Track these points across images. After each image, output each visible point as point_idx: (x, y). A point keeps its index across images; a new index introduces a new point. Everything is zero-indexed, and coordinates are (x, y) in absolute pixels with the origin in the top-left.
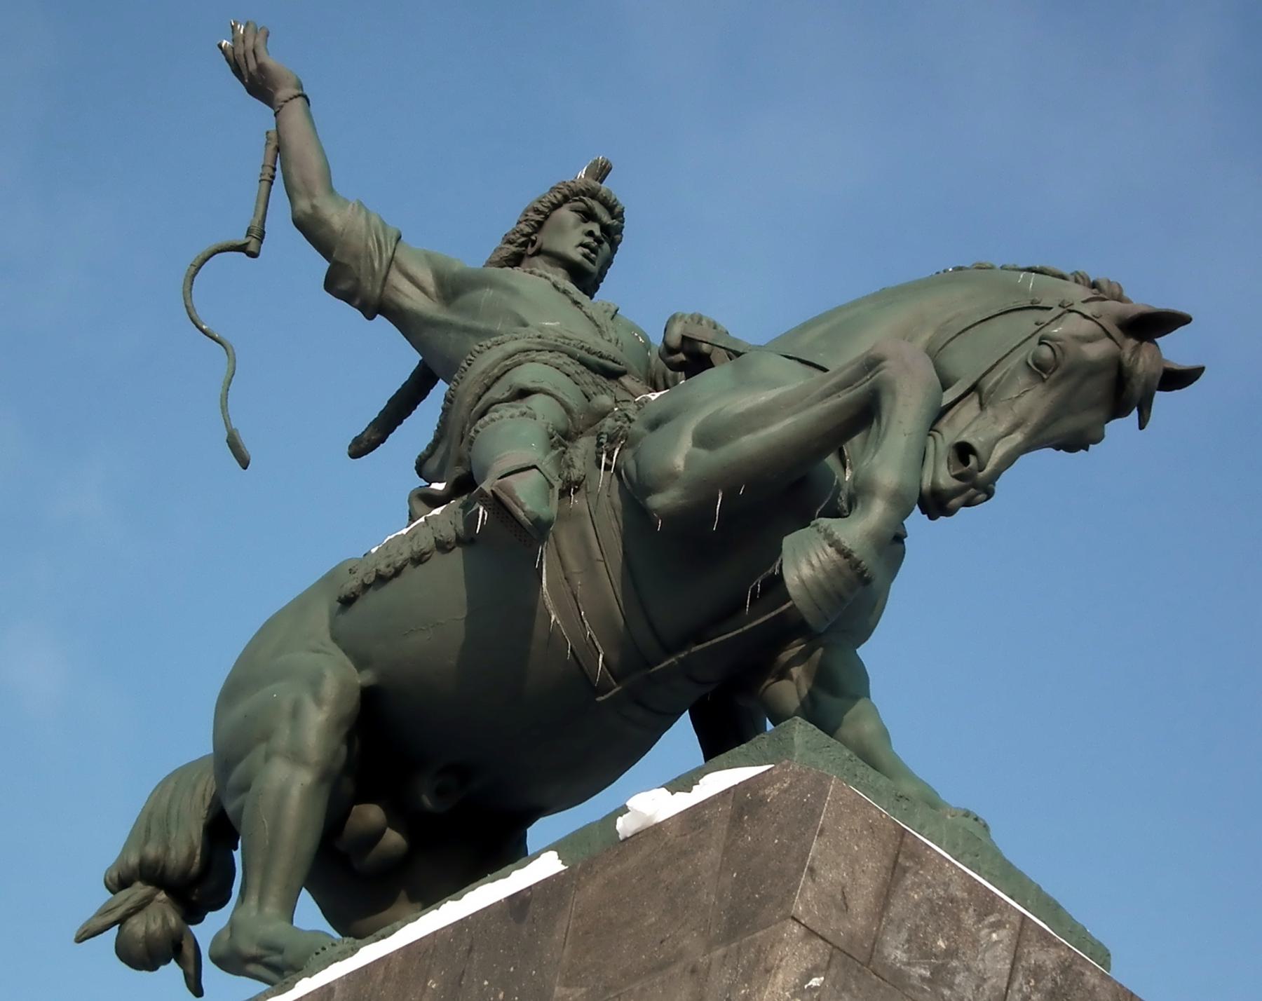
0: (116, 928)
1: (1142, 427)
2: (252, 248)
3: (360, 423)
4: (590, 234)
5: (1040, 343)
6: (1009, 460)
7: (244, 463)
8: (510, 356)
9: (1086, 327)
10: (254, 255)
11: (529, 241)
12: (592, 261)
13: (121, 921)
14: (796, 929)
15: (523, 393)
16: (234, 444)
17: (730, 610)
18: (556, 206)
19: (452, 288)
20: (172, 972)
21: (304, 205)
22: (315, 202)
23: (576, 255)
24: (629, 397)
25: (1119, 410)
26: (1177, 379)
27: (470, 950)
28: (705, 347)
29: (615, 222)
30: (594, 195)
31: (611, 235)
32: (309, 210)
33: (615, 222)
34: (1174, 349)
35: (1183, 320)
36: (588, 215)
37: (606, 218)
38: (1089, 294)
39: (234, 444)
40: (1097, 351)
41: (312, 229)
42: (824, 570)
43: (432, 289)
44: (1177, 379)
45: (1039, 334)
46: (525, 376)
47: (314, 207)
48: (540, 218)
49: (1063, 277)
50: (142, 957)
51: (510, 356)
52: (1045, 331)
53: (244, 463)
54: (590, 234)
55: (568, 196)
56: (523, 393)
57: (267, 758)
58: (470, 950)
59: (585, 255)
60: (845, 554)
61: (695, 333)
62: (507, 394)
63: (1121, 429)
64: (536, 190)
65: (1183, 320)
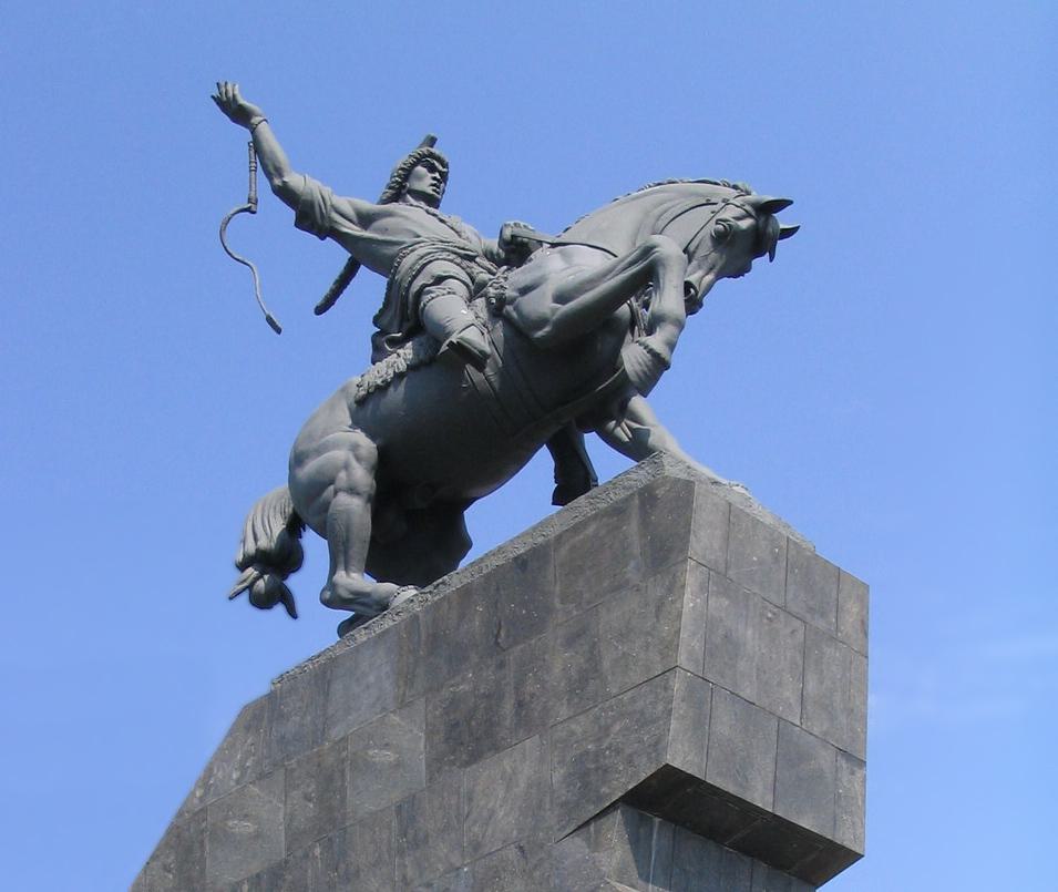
0: (247, 591)
1: (771, 261)
2: (253, 209)
3: (319, 301)
4: (434, 179)
5: (717, 224)
6: (710, 287)
7: (278, 331)
8: (422, 258)
9: (739, 212)
10: (254, 213)
11: (401, 186)
12: (438, 193)
13: (250, 587)
14: (693, 563)
15: (439, 280)
16: (270, 321)
17: (568, 379)
18: (414, 165)
19: (365, 220)
20: (280, 609)
21: (277, 182)
22: (285, 179)
23: (430, 190)
24: (492, 277)
25: (760, 254)
26: (787, 233)
27: (498, 589)
28: (525, 240)
29: (445, 170)
30: (431, 155)
31: (444, 176)
32: (280, 184)
33: (445, 170)
34: (783, 220)
35: (790, 202)
36: (432, 169)
37: (440, 168)
38: (736, 193)
39: (270, 321)
40: (745, 224)
41: (286, 194)
42: (647, 366)
43: (355, 219)
44: (787, 233)
45: (714, 219)
46: (439, 268)
47: (284, 182)
48: (407, 173)
49: (716, 184)
50: (262, 602)
51: (422, 258)
52: (718, 217)
53: (278, 331)
54: (434, 179)
55: (420, 160)
56: (439, 280)
57: (336, 493)
58: (498, 589)
59: (434, 190)
60: (651, 351)
61: (517, 231)
62: (432, 281)
63: (759, 263)
64: (402, 159)
65: (790, 202)
